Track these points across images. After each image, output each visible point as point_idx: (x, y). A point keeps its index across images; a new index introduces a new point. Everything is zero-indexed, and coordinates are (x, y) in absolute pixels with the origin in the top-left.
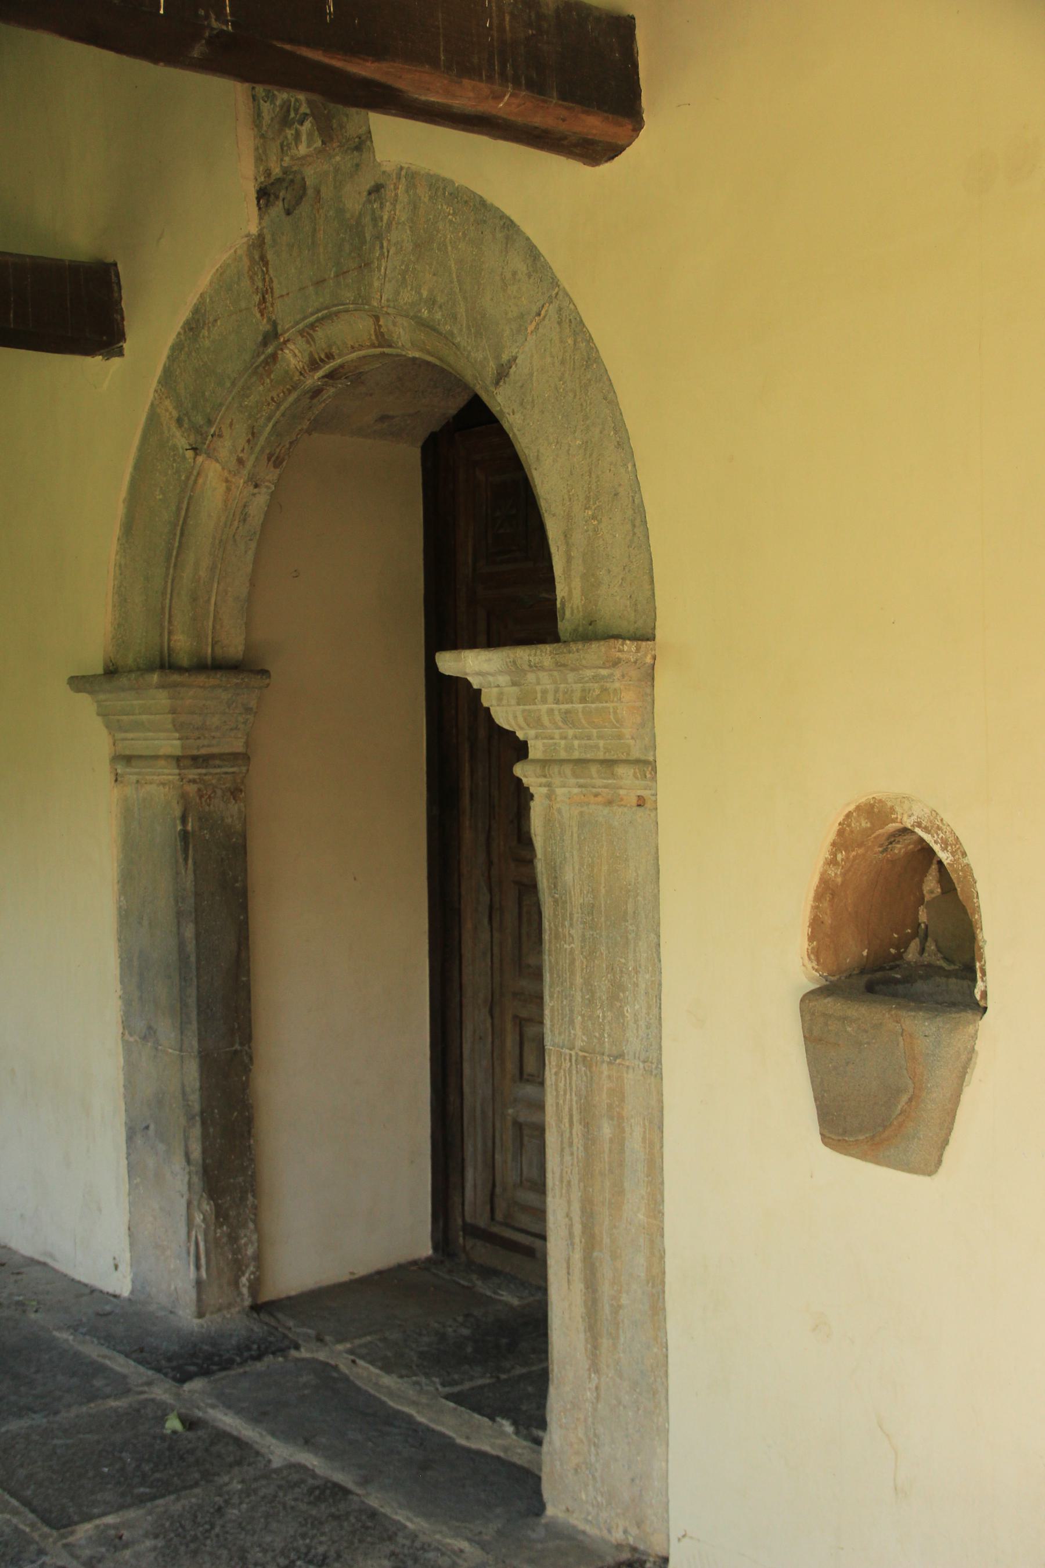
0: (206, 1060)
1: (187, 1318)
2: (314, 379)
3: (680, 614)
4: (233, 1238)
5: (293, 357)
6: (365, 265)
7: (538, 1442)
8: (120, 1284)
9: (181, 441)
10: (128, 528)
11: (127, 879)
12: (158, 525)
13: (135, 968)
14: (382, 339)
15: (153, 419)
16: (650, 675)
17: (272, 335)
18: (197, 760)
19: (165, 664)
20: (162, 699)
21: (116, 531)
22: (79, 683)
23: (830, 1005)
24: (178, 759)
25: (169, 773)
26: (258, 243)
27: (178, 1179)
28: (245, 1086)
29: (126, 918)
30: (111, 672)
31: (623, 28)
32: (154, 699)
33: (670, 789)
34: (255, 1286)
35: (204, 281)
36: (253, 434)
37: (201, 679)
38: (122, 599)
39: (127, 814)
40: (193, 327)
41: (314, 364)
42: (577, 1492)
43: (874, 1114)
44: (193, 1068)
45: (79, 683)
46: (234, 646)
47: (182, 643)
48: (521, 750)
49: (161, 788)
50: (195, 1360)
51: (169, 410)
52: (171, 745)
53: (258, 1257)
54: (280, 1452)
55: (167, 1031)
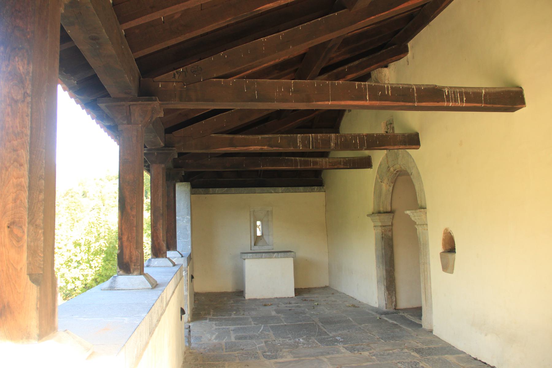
0: (386, 270)
1: (384, 309)
2: (395, 172)
3: (429, 205)
4: (391, 298)
5: (392, 169)
6: (397, 159)
7: (421, 319)
8: (377, 306)
9: (380, 181)
10: (374, 192)
11: (376, 244)
12: (378, 193)
13: (377, 257)
14: (401, 168)
15: (376, 177)
16: (426, 213)
17: (389, 167)
18: (384, 226)
19: (379, 212)
20: (378, 217)
21: (373, 193)
22: (368, 215)
23: (444, 254)
24: (381, 226)
25: (380, 228)
26: (386, 154)
27: (383, 288)
28: (394, 275)
29: (376, 250)
30: (373, 213)
31: (417, 135)
32: (377, 217)
33: (429, 227)
34: (396, 305)
35: (381, 159)
36: (388, 180)
37: (383, 214)
38: (374, 204)
39: (376, 234)
40: (380, 165)
41: (394, 170)
42: (425, 325)
43: (447, 267)
44: (384, 272)
45: (368, 215)
46: (389, 209)
47: (381, 209)
48: (415, 223)
49: (379, 230)
50: (386, 313)
51: (378, 177)
52: (380, 224)
53: (396, 301)
54: (391, 321)
55: (381, 267)
